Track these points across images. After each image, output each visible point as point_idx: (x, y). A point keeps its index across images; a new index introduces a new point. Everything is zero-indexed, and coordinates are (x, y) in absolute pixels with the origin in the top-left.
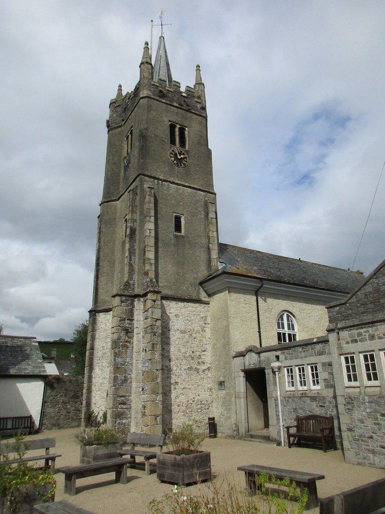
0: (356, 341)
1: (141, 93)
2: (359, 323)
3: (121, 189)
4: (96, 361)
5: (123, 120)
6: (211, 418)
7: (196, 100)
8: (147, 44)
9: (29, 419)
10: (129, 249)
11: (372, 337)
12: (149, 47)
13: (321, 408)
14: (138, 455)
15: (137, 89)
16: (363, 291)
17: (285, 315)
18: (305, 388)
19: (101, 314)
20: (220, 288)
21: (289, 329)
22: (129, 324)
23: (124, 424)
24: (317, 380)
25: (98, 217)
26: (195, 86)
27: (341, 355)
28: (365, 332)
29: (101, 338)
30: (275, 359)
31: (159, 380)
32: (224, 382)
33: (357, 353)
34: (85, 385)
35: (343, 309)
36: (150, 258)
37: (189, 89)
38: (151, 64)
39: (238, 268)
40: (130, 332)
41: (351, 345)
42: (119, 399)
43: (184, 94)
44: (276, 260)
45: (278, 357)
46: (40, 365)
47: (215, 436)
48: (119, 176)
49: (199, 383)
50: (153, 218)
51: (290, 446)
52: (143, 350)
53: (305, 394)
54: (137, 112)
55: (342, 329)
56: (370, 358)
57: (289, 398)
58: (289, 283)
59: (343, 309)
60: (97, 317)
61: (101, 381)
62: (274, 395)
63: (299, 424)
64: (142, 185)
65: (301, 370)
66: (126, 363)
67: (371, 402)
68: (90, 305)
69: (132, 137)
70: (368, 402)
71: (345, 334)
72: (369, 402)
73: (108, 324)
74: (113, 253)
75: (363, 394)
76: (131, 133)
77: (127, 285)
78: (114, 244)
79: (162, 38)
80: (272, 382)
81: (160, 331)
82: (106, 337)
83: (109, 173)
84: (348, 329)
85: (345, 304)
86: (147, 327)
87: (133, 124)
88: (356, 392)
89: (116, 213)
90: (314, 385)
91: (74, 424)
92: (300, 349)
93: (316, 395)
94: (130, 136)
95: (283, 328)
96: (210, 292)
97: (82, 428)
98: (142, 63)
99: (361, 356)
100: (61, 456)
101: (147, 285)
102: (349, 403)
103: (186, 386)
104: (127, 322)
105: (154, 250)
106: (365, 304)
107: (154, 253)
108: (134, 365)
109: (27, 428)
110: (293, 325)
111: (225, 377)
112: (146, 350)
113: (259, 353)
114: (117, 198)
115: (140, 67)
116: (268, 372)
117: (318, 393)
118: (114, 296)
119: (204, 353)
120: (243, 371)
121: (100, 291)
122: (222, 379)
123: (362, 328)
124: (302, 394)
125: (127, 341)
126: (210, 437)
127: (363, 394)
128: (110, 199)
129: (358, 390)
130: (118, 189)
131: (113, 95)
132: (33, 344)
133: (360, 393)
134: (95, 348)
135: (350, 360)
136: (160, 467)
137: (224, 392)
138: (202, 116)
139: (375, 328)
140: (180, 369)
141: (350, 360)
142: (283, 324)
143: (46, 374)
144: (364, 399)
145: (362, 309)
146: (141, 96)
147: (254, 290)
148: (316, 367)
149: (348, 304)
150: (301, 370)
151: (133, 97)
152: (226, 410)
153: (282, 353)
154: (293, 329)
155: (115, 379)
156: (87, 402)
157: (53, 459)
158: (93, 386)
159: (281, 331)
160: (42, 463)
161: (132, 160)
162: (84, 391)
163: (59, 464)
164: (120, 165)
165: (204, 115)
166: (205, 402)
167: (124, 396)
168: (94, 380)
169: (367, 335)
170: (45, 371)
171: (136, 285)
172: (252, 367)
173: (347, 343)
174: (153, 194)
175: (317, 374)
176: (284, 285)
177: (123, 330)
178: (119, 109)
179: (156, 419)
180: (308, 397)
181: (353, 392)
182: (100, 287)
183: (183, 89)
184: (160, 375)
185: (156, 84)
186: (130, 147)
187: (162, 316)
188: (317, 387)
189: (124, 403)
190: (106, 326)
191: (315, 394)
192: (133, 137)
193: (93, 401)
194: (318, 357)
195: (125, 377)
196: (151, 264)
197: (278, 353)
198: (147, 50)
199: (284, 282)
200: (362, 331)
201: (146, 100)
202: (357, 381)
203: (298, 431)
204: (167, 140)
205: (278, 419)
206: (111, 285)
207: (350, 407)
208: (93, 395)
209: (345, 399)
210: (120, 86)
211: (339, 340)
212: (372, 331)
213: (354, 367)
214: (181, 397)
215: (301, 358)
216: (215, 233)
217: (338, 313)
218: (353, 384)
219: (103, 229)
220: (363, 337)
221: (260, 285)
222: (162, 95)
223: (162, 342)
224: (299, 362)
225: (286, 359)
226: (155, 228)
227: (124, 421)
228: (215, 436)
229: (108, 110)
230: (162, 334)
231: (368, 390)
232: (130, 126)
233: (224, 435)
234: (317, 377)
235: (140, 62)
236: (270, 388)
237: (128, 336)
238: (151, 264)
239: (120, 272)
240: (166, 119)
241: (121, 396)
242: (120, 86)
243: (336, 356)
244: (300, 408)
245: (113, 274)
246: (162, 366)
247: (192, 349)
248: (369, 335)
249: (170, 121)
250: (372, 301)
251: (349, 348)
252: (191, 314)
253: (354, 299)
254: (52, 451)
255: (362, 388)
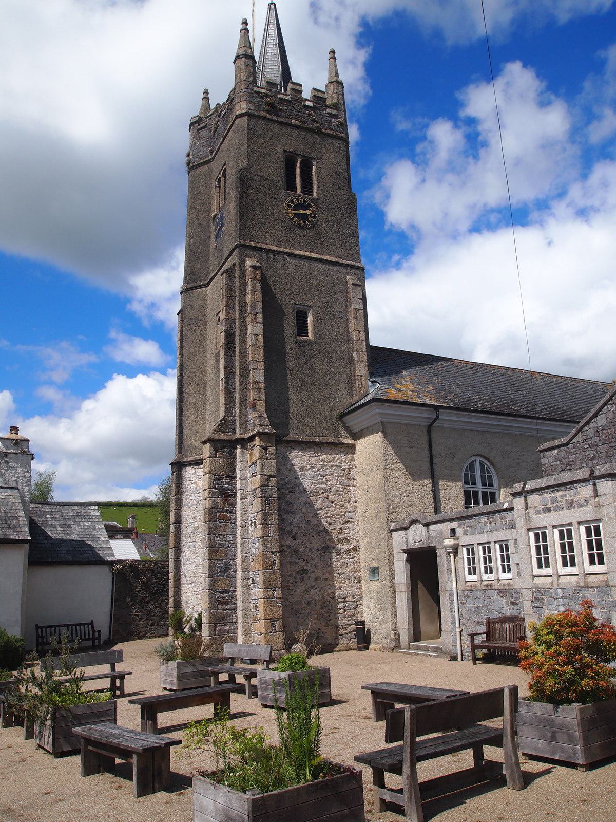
0: (549, 510)
1: (237, 107)
2: (553, 483)
3: (211, 268)
4: (184, 538)
5: (212, 151)
6: (359, 622)
7: (329, 110)
8: (245, 23)
9: (90, 626)
10: (225, 368)
11: (571, 505)
12: (249, 27)
13: (512, 606)
14: (238, 673)
15: (231, 100)
16: (591, 425)
17: (478, 462)
18: (491, 577)
19: (188, 468)
20: (370, 424)
21: (484, 484)
22: (228, 484)
23: (228, 632)
24: (509, 566)
25: (178, 315)
26: (327, 86)
27: (529, 530)
28: (561, 496)
29: (190, 504)
30: (449, 534)
31: (276, 567)
32: (377, 568)
33: (550, 528)
34: (171, 576)
35: (563, 454)
36: (258, 380)
37: (316, 93)
38: (253, 58)
39: (400, 391)
40: (231, 497)
41: (542, 515)
42: (217, 596)
43: (308, 103)
44: (470, 371)
45: (453, 531)
46: (104, 546)
47: (367, 648)
48: (209, 245)
49: (340, 571)
50: (261, 315)
51: (475, 660)
52: (252, 523)
53: (491, 585)
54: (231, 139)
55: (532, 491)
56: (593, 531)
57: (467, 592)
58: (482, 412)
59: (563, 454)
60: (184, 473)
61: (194, 569)
62: (448, 588)
63: (489, 630)
64: (242, 263)
65: (487, 550)
66: (227, 543)
67: (566, 597)
68: (173, 456)
69: (225, 180)
70: (561, 598)
71: (534, 499)
72: (562, 597)
73: (200, 484)
74: (203, 372)
75: (555, 585)
76: (224, 175)
77: (225, 425)
78: (204, 357)
79: (272, 6)
80: (446, 568)
81: (276, 495)
82: (198, 504)
83: (192, 240)
84: (540, 493)
85: (566, 445)
86: (255, 489)
87: (225, 159)
88: (546, 584)
89: (205, 307)
90: (504, 572)
91: (160, 633)
92: (485, 519)
93: (506, 587)
94: (223, 179)
95: (474, 483)
96: (356, 429)
97: (170, 638)
98: (237, 57)
99: (582, 528)
100: (132, 673)
101: (254, 423)
102: (537, 599)
103: (321, 575)
104: (225, 480)
105: (263, 367)
106: (594, 446)
107: (262, 371)
108: (239, 545)
109: (89, 639)
110: (490, 478)
111: (378, 560)
112: (255, 523)
113: (427, 525)
114: (206, 282)
115: (234, 63)
116: (441, 554)
117: (509, 584)
118: (204, 443)
119: (348, 525)
120: (405, 551)
121: (186, 432)
122: (375, 564)
123: (557, 491)
124: (471, 586)
125: (227, 511)
126: (359, 649)
127: (555, 585)
128: (194, 285)
129: (549, 580)
130: (208, 267)
131: (195, 110)
132: (93, 513)
133: (552, 584)
134: (183, 520)
135: (541, 536)
136: (261, 688)
137: (378, 583)
138: (340, 139)
139: (575, 490)
140: (310, 550)
141: (541, 536)
142: (473, 476)
143: (114, 559)
144: (556, 594)
145: (591, 453)
146: (237, 113)
147: (424, 426)
148: (507, 546)
149: (570, 446)
150: (487, 550)
151: (225, 113)
152: (381, 610)
153: (460, 525)
154: (491, 485)
155: (212, 568)
156: (174, 600)
157: (122, 677)
158: (182, 577)
159: (471, 488)
160: (106, 683)
161: (226, 221)
162: (170, 583)
163: (130, 686)
164: (209, 227)
165: (343, 135)
166: (350, 599)
167: (226, 592)
168: (183, 568)
169: (564, 500)
170: (113, 555)
171: (238, 423)
172: (418, 545)
173: (538, 512)
174: (259, 277)
175: (508, 556)
176: (474, 414)
177: (221, 493)
178: (204, 133)
179: (273, 624)
180: (495, 590)
181: (543, 583)
182: (186, 425)
183: (306, 94)
184: (277, 560)
185: (261, 90)
186: (222, 197)
187: (278, 470)
188: (508, 576)
189: (227, 603)
190: (197, 486)
191: (504, 585)
192: (227, 182)
193: (184, 598)
194: (509, 531)
195: (226, 563)
196: (259, 390)
197: (455, 525)
198: (245, 33)
199: (475, 411)
200: (558, 494)
201: (245, 119)
202: (604, 564)
203: (488, 639)
204: (280, 181)
205: (453, 623)
206: (202, 422)
207: (537, 604)
208: (184, 589)
209: (533, 593)
210: (206, 92)
211: (527, 508)
212: (570, 496)
213: (571, 545)
214: (313, 591)
215: (487, 532)
216: (362, 334)
217: (557, 459)
218: (544, 571)
219: (187, 334)
220: (559, 503)
221: (435, 417)
222: (273, 109)
223: (279, 510)
224: (483, 538)
225: (465, 534)
226: (264, 330)
227: (227, 628)
228: (367, 648)
229: (189, 133)
230: (279, 498)
231: (562, 579)
232: (223, 162)
233: (378, 647)
234: (508, 560)
235: (235, 55)
236: (442, 578)
237: (228, 503)
238: (259, 390)
239: (214, 402)
240: (279, 149)
241: (222, 592)
242: (206, 92)
243: (523, 532)
244: (484, 606)
245: (204, 405)
246: (281, 545)
247: (329, 520)
248: (567, 501)
249: (285, 151)
250: (605, 440)
251: (541, 520)
252: (326, 466)
253: (579, 438)
254: (119, 667)
255: (555, 578)
